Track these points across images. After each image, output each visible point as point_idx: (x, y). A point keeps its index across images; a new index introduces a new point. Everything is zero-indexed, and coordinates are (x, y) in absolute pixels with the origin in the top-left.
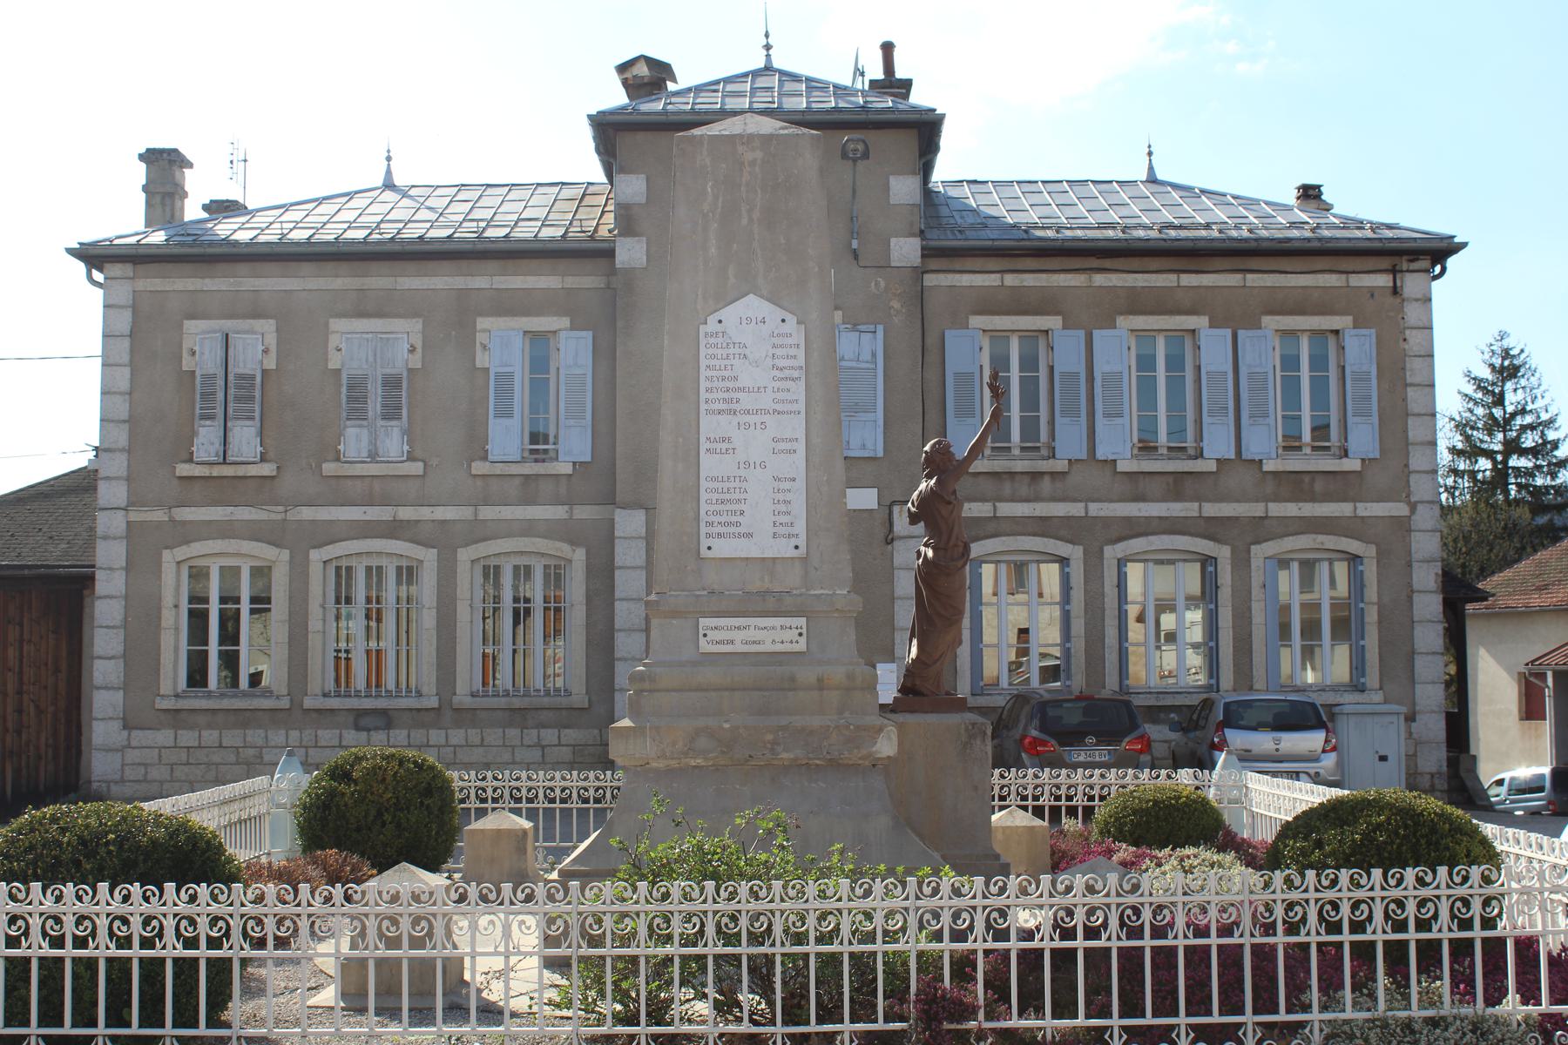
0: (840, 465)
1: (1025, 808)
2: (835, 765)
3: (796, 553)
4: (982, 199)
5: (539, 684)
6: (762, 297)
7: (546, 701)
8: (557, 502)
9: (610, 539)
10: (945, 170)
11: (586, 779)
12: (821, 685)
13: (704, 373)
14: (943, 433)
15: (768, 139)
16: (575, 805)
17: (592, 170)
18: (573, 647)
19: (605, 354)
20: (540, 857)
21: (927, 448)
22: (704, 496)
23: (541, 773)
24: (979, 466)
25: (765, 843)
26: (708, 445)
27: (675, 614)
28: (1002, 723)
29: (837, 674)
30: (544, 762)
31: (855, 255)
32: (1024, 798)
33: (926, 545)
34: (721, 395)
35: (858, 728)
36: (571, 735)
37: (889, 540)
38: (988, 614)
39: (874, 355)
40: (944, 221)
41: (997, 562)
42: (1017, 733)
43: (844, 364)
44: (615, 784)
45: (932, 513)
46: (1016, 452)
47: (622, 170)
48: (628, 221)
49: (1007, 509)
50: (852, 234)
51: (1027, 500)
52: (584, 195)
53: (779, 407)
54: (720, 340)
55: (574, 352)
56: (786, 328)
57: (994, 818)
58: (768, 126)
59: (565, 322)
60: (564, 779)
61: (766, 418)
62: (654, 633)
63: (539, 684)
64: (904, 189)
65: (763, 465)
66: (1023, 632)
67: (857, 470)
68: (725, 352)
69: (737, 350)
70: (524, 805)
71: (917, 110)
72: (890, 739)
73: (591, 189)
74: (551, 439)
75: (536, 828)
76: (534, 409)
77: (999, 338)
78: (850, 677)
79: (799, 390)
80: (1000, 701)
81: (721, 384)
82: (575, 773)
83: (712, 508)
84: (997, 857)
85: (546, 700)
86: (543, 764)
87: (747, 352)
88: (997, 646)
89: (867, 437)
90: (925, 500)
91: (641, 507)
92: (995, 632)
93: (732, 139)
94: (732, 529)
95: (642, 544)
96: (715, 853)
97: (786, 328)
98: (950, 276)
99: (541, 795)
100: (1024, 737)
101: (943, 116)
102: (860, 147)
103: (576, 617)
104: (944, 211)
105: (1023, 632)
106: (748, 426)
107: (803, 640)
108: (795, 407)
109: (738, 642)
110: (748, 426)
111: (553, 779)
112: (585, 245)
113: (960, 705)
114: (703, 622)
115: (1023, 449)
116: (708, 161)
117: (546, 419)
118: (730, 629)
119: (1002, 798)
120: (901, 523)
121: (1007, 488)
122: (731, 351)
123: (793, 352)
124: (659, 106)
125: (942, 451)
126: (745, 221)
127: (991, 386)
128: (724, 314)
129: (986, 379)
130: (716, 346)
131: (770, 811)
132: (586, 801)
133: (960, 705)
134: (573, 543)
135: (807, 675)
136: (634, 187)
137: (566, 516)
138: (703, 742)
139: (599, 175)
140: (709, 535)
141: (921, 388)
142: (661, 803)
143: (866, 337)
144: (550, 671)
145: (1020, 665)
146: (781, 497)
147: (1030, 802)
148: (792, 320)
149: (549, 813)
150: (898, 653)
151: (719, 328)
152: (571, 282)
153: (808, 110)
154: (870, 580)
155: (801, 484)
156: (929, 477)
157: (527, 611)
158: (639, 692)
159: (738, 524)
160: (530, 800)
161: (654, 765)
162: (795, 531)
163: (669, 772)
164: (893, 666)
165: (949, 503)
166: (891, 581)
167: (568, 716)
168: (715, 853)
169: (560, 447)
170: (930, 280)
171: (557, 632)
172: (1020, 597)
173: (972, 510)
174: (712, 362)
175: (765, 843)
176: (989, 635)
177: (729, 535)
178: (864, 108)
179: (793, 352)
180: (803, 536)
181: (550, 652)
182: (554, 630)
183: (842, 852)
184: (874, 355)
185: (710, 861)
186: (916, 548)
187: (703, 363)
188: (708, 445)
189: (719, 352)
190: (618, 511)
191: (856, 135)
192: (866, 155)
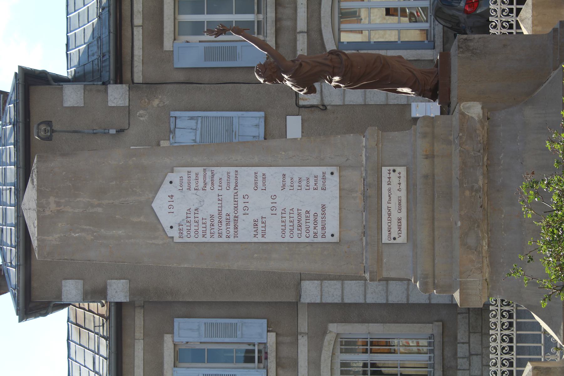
0: (272, 143)
1: (519, 11)
2: (488, 147)
3: (336, 174)
4: (80, 40)
5: (426, 357)
6: (154, 197)
7: (438, 352)
8: (295, 343)
9: (322, 305)
10: (59, 67)
11: (495, 324)
12: (431, 156)
13: (208, 239)
14: (250, 69)
15: (41, 193)
16: (514, 332)
17: (60, 317)
18: (398, 333)
19: (191, 309)
20: (552, 357)
21: (262, 80)
22: (296, 239)
23: (491, 356)
24: (271, 41)
25: (546, 197)
26: (259, 236)
27: (379, 259)
28: (454, 28)
29: (422, 145)
30: (482, 354)
31: (120, 131)
32: (511, 11)
33: (331, 82)
34: (224, 227)
35: (461, 130)
36: (462, 335)
37: (323, 108)
38: (377, 37)
39: (192, 118)
40: (96, 67)
41: (340, 31)
42: (462, 16)
43: (198, 139)
44: (499, 303)
45: (308, 78)
46: (261, 17)
47: (59, 297)
48: (96, 293)
49: (302, 24)
50: (106, 133)
51: (295, 9)
52: (77, 324)
53: (232, 185)
54: (185, 228)
55: (189, 331)
56: (177, 181)
57: (525, 32)
58: (31, 193)
59: (168, 338)
60: (495, 340)
61: (240, 194)
62: (393, 275)
63: (426, 357)
64: (73, 96)
65: (274, 197)
66: (389, 12)
67: (273, 131)
68: (193, 224)
69: (192, 215)
70: (514, 369)
71: (16, 86)
72: (469, 108)
73: (73, 319)
74: (251, 347)
75: (531, 360)
76: (229, 360)
77: (180, 29)
78: (425, 135)
79: (221, 172)
80: (439, 28)
81: (216, 226)
82: (491, 332)
83: (304, 233)
84: (555, 30)
85: (436, 352)
86: (484, 354)
87: (193, 208)
88: (399, 31)
89: (250, 123)
90: (298, 83)
91: (299, 284)
92: (388, 32)
93: (40, 219)
94: (319, 219)
95: (326, 283)
96: (553, 232)
97: (177, 181)
98: (136, 64)
99: (507, 356)
100: (465, 11)
101: (20, 67)
102: (43, 127)
103: (377, 330)
104: (89, 67)
105: (389, 12)
106: (246, 208)
107: (398, 169)
108: (233, 174)
109: (399, 215)
110: (246, 208)
111: (495, 348)
112: (113, 324)
113: (445, 55)
114: (385, 240)
115: (259, 12)
116: (56, 236)
117: (237, 351)
118: (390, 221)
119: (511, 27)
120: (313, 99)
121: (287, 23)
122: (192, 219)
123: (193, 176)
124: (13, 271)
125: (264, 70)
126: (100, 210)
127: (217, 35)
128: (166, 224)
129: (212, 38)
130: (189, 230)
131: (522, 193)
132: (511, 324)
133: (445, 55)
134: (325, 332)
135: (423, 167)
136: (71, 289)
137: (306, 337)
138: (471, 241)
139: (63, 314)
140: (323, 236)
141: (214, 85)
142: (516, 271)
143: (179, 124)
144: (415, 349)
145: (412, 14)
146: (296, 185)
147: (514, 7)
148: (170, 177)
149: (520, 351)
150: (404, 102)
151: (176, 228)
152: (139, 333)
153: (16, 164)
154: (355, 121)
155: (287, 170)
156: (282, 79)
157: (373, 365)
158: (435, 286)
159: (315, 215)
160: (511, 365)
161: (487, 275)
162: (320, 175)
163: (492, 264)
164: (414, 105)
165: (301, 65)
166: (353, 107)
167: (448, 338)
168: (553, 232)
169: (256, 341)
170: (138, 78)
171: (388, 344)
172: (363, 14)
173: (302, 48)
174: (200, 233)
175: (546, 197)
176: (392, 36)
177: (323, 221)
178: (15, 124)
179: (193, 176)
180: (324, 169)
181: (402, 349)
182: (385, 346)
183: (552, 142)
184: (192, 118)
185: (559, 236)
186: (332, 89)
187: (200, 239)
188: (259, 236)
189: (193, 228)
190: (302, 300)
191: (34, 130)
192: (49, 123)
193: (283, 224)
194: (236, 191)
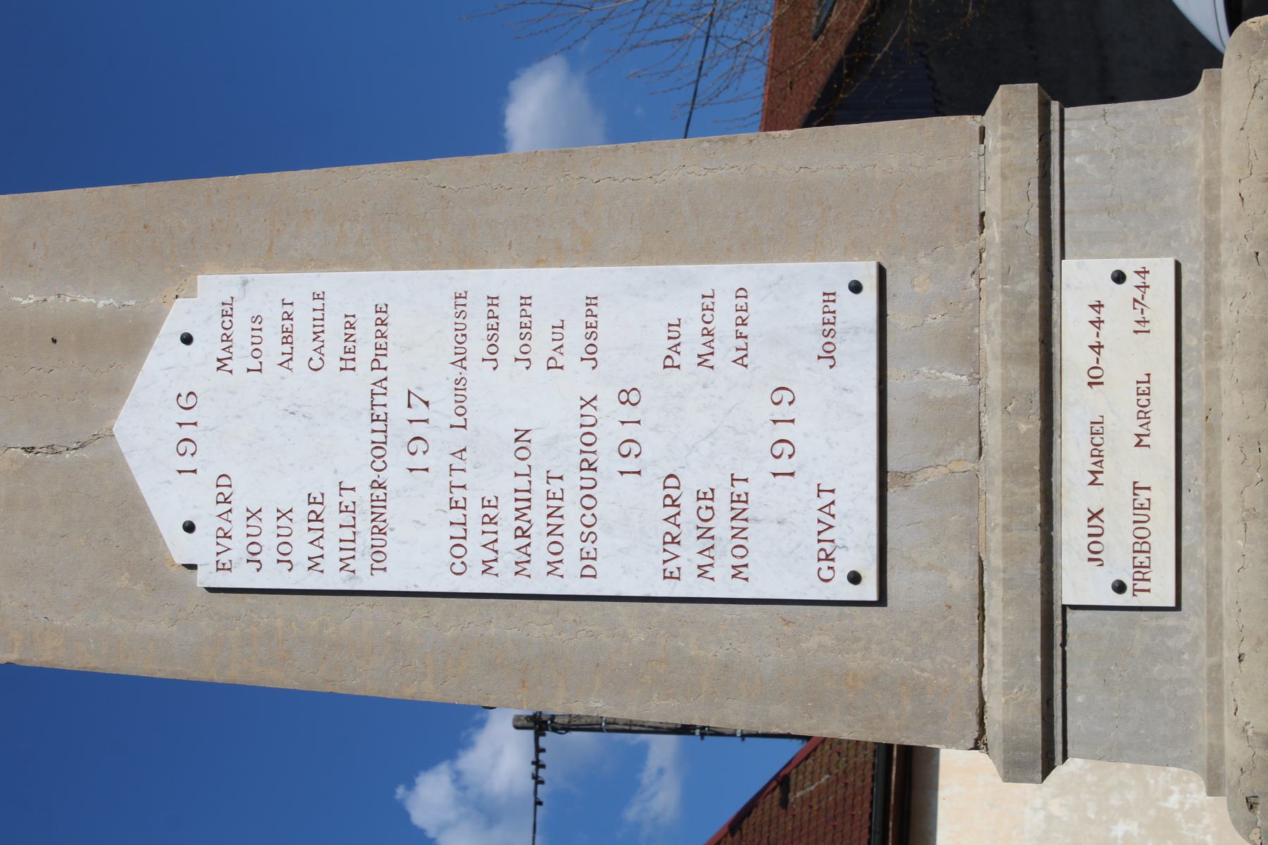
26: (722, 569)
53: (365, 353)
193: (457, 515)
194: (381, 374)
